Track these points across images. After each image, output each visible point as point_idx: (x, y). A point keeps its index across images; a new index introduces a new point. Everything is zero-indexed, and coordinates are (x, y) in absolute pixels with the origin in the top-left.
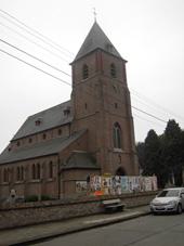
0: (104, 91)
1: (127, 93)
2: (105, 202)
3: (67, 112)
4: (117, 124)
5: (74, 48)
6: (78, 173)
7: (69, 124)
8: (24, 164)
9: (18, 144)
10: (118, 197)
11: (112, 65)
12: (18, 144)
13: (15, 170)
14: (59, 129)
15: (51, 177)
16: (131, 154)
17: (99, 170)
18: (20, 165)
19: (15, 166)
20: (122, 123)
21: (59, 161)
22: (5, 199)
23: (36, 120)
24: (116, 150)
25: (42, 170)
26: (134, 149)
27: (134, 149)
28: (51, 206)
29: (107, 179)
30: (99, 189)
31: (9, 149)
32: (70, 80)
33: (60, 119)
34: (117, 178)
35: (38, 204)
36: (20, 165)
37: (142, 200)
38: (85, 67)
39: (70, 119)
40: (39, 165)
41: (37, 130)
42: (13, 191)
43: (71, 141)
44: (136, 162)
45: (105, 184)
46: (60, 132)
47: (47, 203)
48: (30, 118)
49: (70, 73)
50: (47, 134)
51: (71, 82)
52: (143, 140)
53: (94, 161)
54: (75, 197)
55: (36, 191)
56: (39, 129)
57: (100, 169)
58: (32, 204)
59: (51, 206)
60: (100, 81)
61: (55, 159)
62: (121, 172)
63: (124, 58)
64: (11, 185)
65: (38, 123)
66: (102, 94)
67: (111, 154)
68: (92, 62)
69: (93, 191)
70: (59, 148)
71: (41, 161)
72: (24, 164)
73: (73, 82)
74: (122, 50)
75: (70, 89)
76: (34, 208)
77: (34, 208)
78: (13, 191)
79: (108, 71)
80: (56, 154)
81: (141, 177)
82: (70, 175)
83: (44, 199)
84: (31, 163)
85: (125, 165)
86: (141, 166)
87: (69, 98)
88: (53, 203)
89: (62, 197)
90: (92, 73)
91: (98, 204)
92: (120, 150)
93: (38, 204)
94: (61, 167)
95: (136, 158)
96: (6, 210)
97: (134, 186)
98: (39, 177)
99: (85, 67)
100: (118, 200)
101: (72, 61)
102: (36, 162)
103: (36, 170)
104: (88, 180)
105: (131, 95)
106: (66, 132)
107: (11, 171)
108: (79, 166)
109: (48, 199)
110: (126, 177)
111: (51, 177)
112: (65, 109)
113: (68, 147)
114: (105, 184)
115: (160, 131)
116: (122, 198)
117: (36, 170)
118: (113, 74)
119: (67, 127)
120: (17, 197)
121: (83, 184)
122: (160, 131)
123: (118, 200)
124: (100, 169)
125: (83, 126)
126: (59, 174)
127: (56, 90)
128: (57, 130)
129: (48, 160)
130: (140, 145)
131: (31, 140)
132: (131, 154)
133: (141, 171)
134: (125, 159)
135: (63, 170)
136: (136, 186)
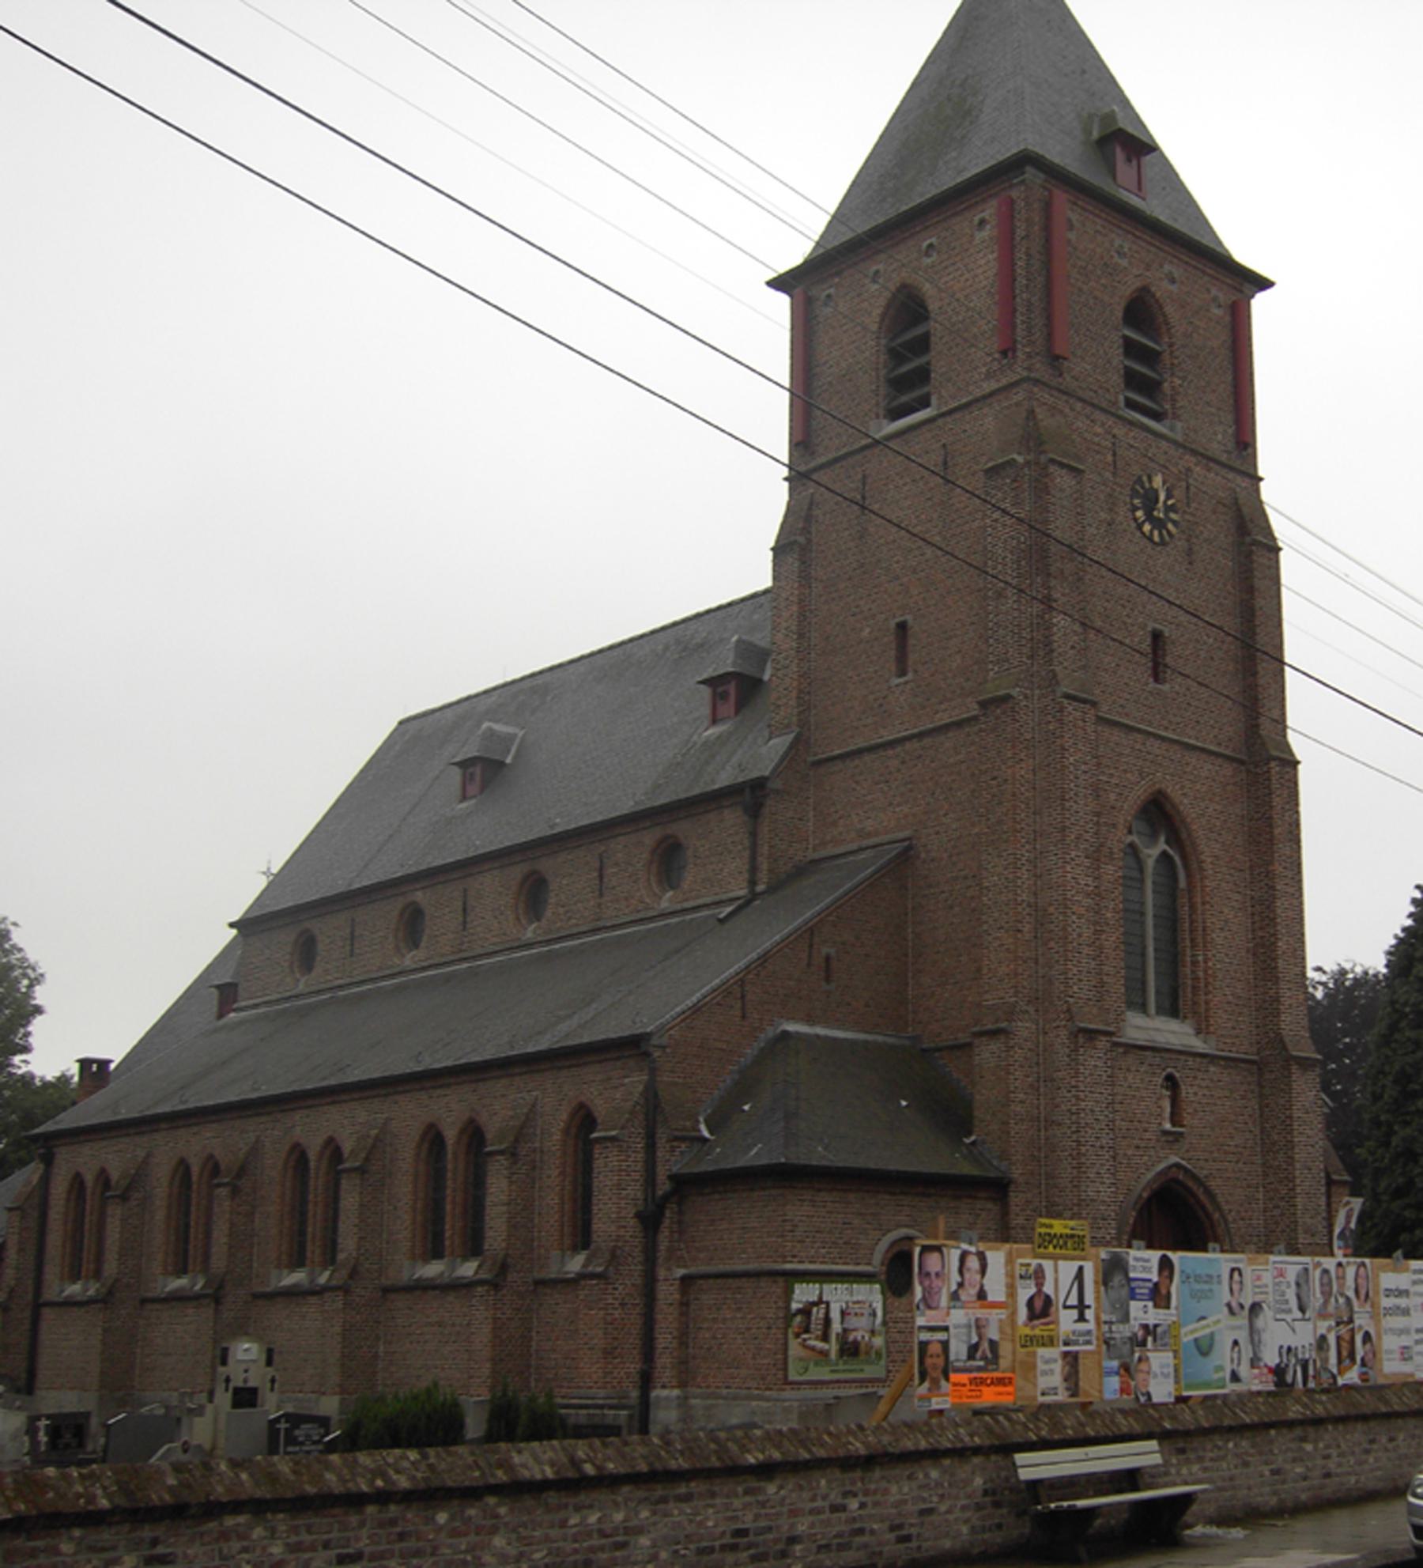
0: (1061, 526)
1: (1252, 550)
2: (1033, 1466)
3: (737, 690)
4: (1158, 813)
5: (811, 139)
6: (803, 1211)
7: (751, 795)
8: (347, 1125)
9: (306, 953)
10: (1144, 1420)
11: (1140, 311)
12: (306, 953)
13: (406, 1159)
14: (662, 831)
15: (582, 1238)
16: (1265, 1067)
17: (988, 1197)
18: (311, 1129)
19: (273, 1137)
20: (1205, 801)
21: (652, 1107)
22: (171, 1424)
23: (464, 750)
24: (1149, 1027)
25: (498, 1187)
26: (1294, 1027)
27: (1294, 1027)
28: (572, 1484)
29: (1060, 1276)
30: (985, 1353)
31: (220, 990)
32: (771, 418)
33: (673, 746)
34: (1144, 1261)
35: (456, 1464)
36: (196, 1144)
37: (1350, 1458)
38: (908, 310)
39: (762, 752)
40: (474, 1135)
41: (476, 840)
42: (246, 1351)
43: (770, 931)
44: (1310, 1141)
45: (1041, 1308)
46: (669, 861)
47: (534, 1460)
48: (415, 737)
49: (778, 361)
50: (329, 932)
51: (778, 438)
52: (1370, 954)
53: (953, 1115)
54: (778, 1413)
55: (448, 1353)
56: (491, 827)
57: (998, 1188)
58: (405, 1466)
59: (572, 1484)
60: (1033, 439)
61: (613, 1093)
62: (1176, 1216)
63: (1243, 251)
64: (230, 1302)
65: (485, 772)
66: (1039, 552)
67: (1094, 1060)
68: (963, 274)
69: (932, 1364)
70: (656, 999)
71: (499, 1107)
72: (347, 1125)
73: (802, 440)
74: (1229, 174)
75: (765, 499)
76: (428, 1496)
77: (428, 1496)
78: (246, 1351)
79: (1098, 359)
80: (632, 1047)
81: (1341, 1265)
82: (738, 1233)
83: (512, 1421)
84: (407, 1117)
85: (1215, 1144)
86: (1352, 1167)
87: (761, 578)
88: (591, 1457)
89: (665, 1416)
90: (963, 365)
91: (976, 1477)
92: (1174, 1033)
93: (456, 1464)
94: (672, 1162)
95: (1308, 1099)
96: (177, 1512)
97: (1286, 1334)
98: (330, 1254)
99: (908, 310)
100: (1144, 1454)
101: (794, 253)
102: (449, 1110)
103: (455, 1170)
104: (898, 1275)
105: (1291, 569)
106: (719, 862)
107: (239, 1177)
108: (819, 1155)
109: (545, 1426)
110: (1217, 1261)
111: (582, 1238)
112: (719, 664)
113: (736, 990)
114: (1041, 1308)
115: (1412, 909)
116: (1182, 1429)
117: (455, 1170)
118: (1145, 383)
119: (732, 818)
120: (272, 1406)
121: (855, 1304)
122: (1412, 909)
123: (1144, 1454)
124: (998, 1188)
125: (870, 814)
126: (650, 1221)
127: (647, 491)
128: (649, 838)
129: (552, 1100)
130: (1349, 991)
131: (413, 925)
132: (1265, 1067)
133: (1349, 1210)
134: (1214, 1100)
135: (685, 1185)
136: (1303, 1337)
